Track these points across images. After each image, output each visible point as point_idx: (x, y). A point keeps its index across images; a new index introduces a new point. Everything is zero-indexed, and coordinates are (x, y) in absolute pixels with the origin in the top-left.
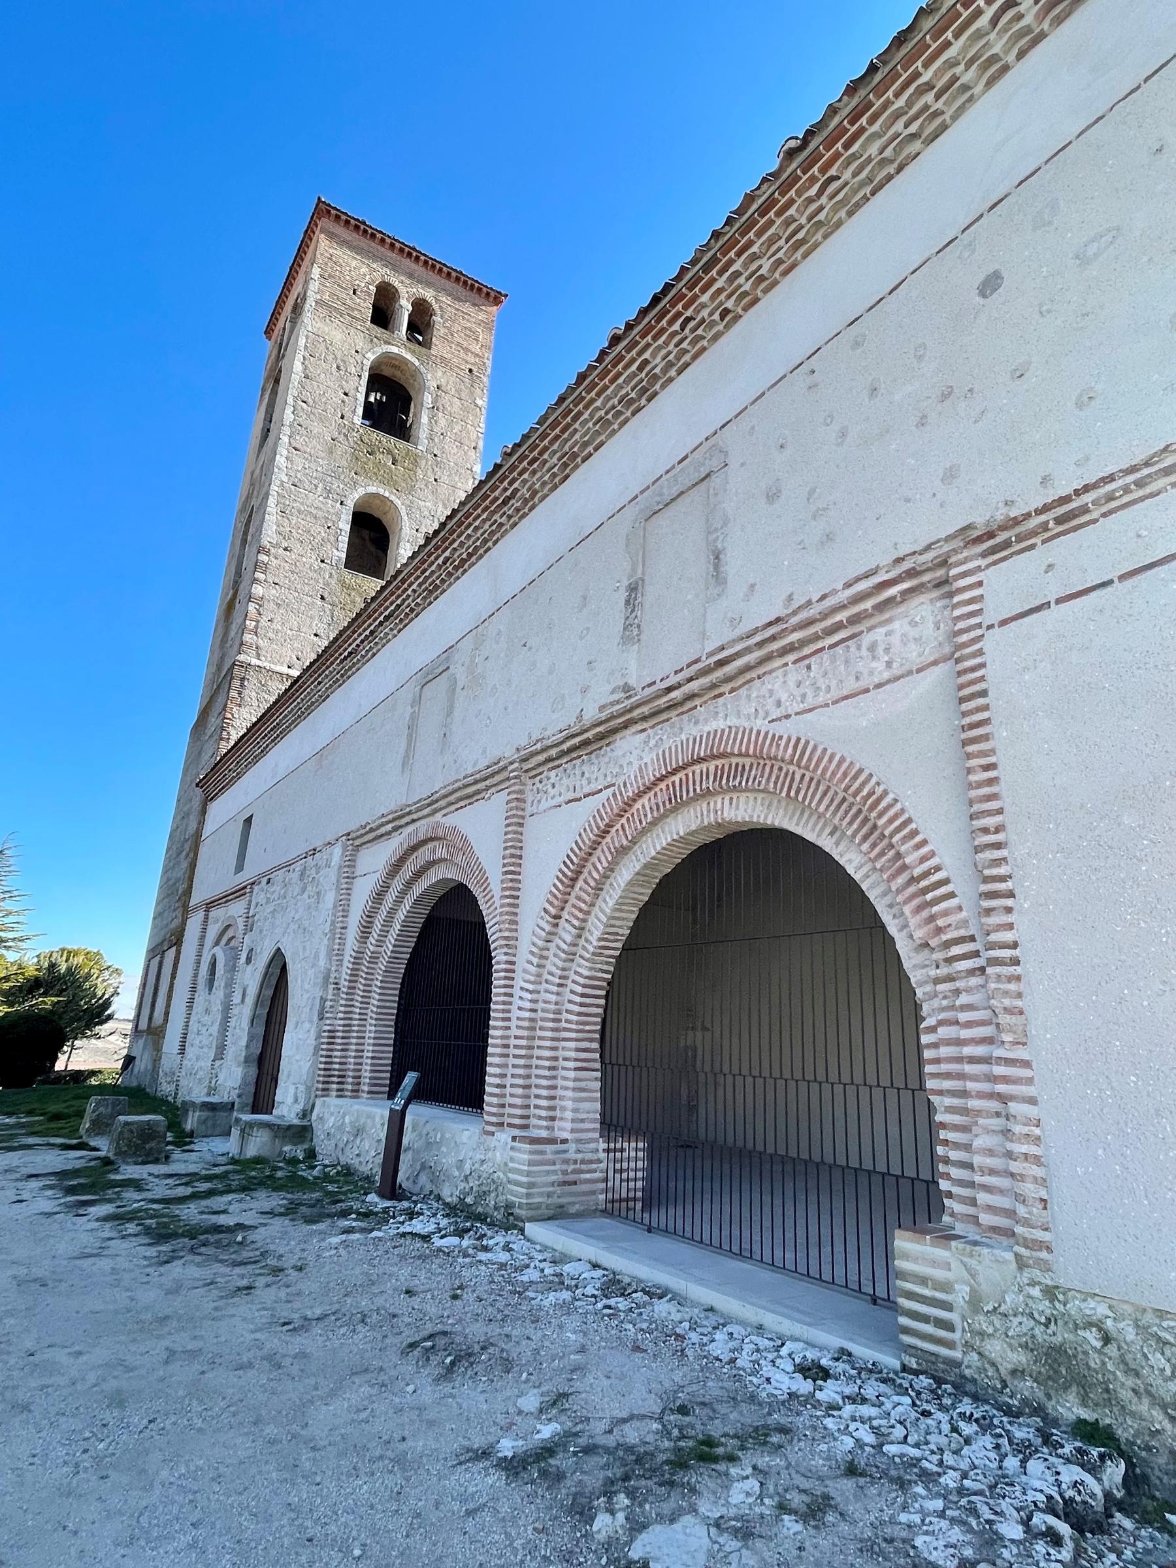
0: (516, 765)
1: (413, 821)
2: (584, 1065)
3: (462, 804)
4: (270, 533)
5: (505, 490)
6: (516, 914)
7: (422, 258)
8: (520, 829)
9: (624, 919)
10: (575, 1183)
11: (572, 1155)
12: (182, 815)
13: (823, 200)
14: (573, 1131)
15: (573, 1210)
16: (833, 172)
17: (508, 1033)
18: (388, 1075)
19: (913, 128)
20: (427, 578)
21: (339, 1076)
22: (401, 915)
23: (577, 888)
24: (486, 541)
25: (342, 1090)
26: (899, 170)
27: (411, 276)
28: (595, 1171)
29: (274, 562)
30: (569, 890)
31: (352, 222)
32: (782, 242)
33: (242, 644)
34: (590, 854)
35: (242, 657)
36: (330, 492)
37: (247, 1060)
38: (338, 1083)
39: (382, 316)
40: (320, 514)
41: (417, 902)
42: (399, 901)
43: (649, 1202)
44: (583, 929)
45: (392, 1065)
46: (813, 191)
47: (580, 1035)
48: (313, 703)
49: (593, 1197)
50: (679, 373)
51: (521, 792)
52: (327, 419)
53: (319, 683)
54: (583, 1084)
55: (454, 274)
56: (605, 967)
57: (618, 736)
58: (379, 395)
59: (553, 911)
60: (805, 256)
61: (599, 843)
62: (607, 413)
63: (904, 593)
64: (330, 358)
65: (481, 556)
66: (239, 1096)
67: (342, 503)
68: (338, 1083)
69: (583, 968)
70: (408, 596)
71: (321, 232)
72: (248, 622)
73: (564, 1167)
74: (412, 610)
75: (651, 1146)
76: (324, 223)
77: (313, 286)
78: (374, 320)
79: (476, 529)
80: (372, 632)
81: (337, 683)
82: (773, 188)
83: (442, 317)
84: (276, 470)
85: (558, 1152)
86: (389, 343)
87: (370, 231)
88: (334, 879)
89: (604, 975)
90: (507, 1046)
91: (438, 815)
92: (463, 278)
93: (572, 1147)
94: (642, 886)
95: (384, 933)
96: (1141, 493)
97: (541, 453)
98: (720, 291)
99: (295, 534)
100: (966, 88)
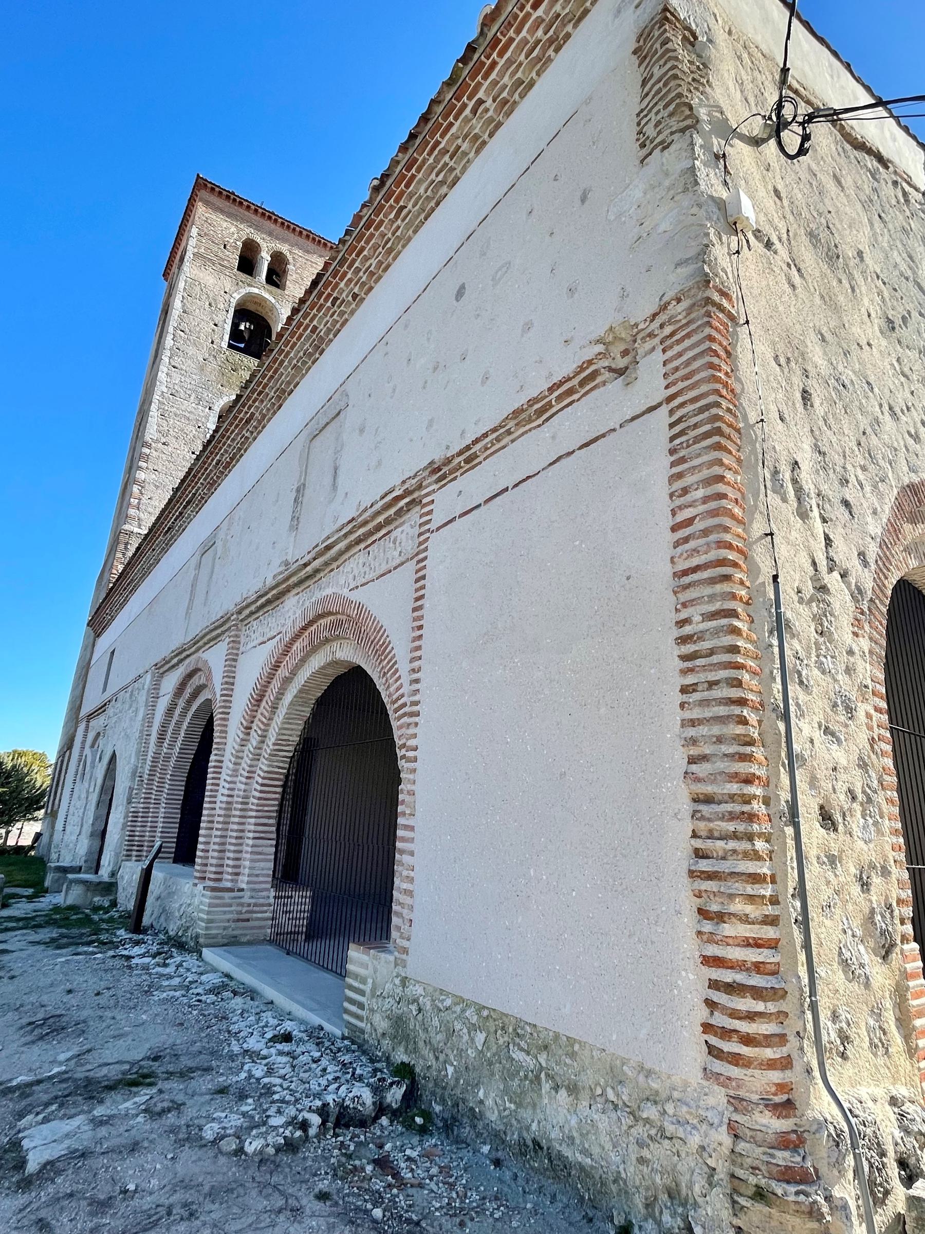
0: (235, 616)
1: (188, 656)
2: (262, 835)
3: (212, 644)
4: (152, 431)
5: (246, 413)
6: (226, 726)
7: (280, 220)
8: (233, 663)
9: (292, 730)
10: (248, 920)
11: (246, 900)
12: (85, 648)
13: (399, 222)
14: (248, 883)
15: (244, 939)
16: (401, 203)
17: (213, 812)
18: (174, 845)
19: (440, 178)
20: (208, 475)
21: (138, 846)
22: (185, 725)
23: (262, 707)
24: (240, 449)
25: (140, 856)
26: (438, 204)
27: (270, 234)
28: (266, 912)
29: (155, 454)
30: (255, 708)
31: (224, 193)
32: (380, 249)
33: (127, 516)
34: (269, 683)
35: (126, 527)
36: (200, 400)
37: (92, 835)
38: (137, 851)
39: (247, 265)
40: (192, 417)
41: (195, 716)
42: (183, 715)
43: (309, 937)
44: (265, 737)
45: (178, 838)
46: (392, 216)
47: (260, 814)
48: (151, 565)
49: (263, 931)
50: (335, 336)
51: (237, 636)
52: (200, 344)
53: (154, 550)
54: (260, 849)
55: (305, 233)
56: (281, 765)
57: (286, 597)
58: (248, 324)
59: (245, 723)
60: (394, 259)
61: (274, 675)
62: (298, 362)
63: (407, 504)
64: (204, 297)
65: (238, 461)
66: (86, 861)
67: (210, 408)
68: (137, 851)
69: (263, 765)
70: (199, 488)
71: (201, 200)
72: (132, 500)
73: (240, 908)
74: (202, 498)
75: (314, 893)
76: (203, 194)
77: (192, 242)
78: (240, 268)
79: (233, 440)
80: (181, 513)
81: (164, 550)
82: (370, 212)
83: (294, 266)
84: (158, 383)
85: (235, 898)
86: (252, 286)
87: (238, 200)
88: (144, 698)
89: (281, 771)
90: (212, 822)
91: (200, 654)
92: (311, 236)
93: (247, 894)
94: (302, 706)
95: (174, 740)
96: (498, 446)
97: (264, 388)
98: (350, 280)
99: (171, 432)
100: (465, 154)
